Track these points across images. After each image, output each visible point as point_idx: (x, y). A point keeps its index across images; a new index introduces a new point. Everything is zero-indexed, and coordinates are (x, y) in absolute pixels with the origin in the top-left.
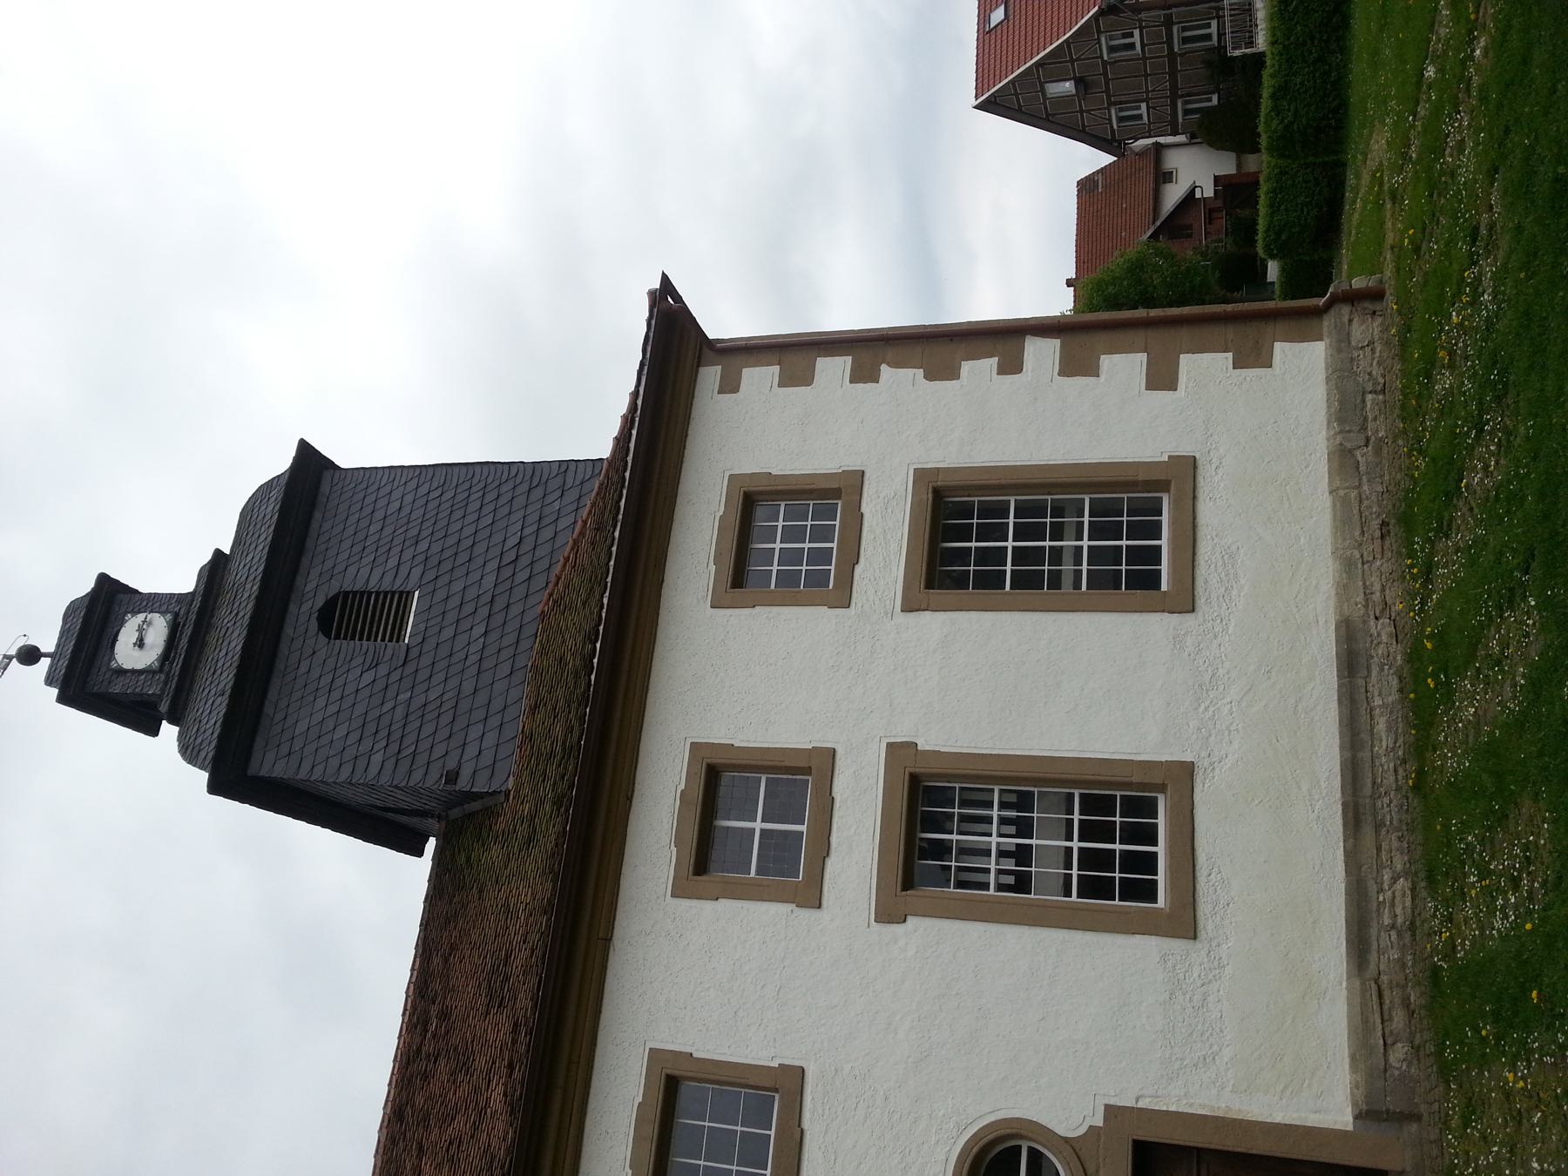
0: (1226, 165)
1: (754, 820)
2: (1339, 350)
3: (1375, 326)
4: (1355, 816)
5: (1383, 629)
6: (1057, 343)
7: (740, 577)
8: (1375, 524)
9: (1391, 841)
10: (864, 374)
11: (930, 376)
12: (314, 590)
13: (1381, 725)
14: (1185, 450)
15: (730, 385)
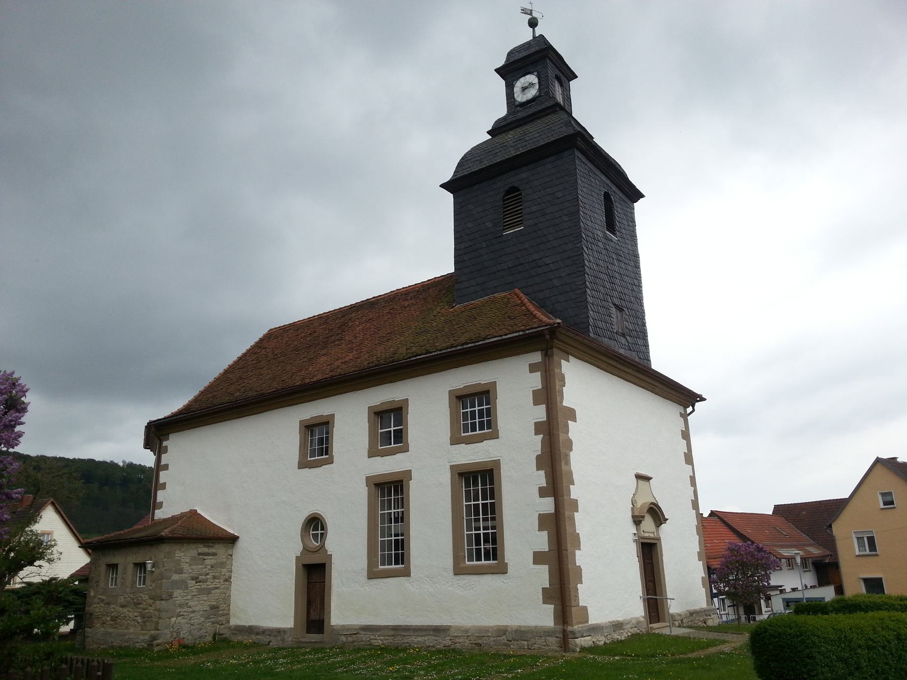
0: (764, 615)
1: (475, 413)
2: (545, 632)
3: (555, 647)
4: (396, 629)
5: (447, 642)
6: (553, 511)
7: (461, 398)
8: (480, 642)
9: (391, 639)
10: (539, 428)
11: (538, 457)
12: (513, 179)
13: (419, 639)
14: (510, 569)
15: (533, 368)
